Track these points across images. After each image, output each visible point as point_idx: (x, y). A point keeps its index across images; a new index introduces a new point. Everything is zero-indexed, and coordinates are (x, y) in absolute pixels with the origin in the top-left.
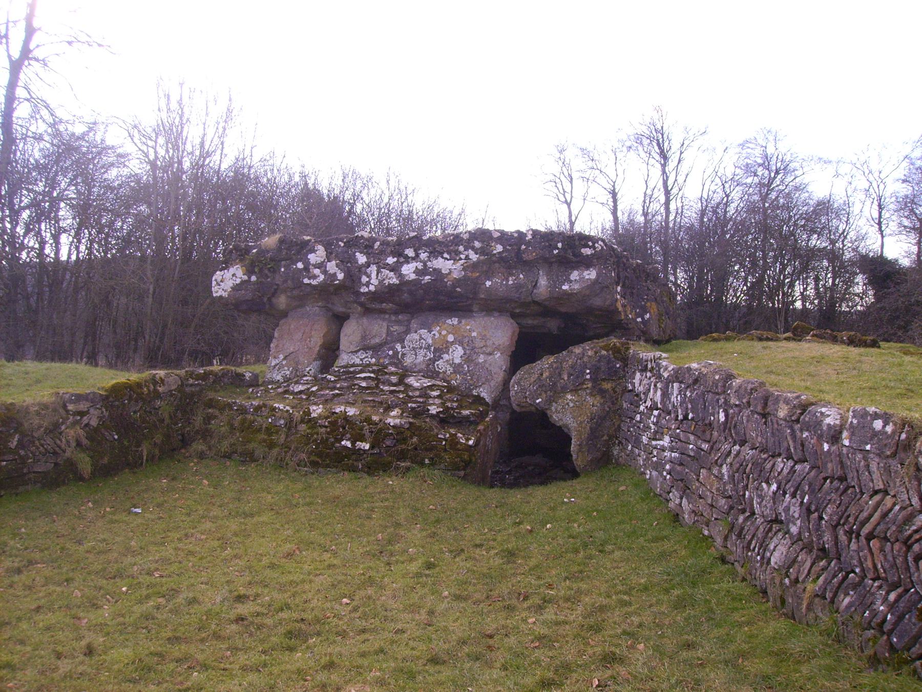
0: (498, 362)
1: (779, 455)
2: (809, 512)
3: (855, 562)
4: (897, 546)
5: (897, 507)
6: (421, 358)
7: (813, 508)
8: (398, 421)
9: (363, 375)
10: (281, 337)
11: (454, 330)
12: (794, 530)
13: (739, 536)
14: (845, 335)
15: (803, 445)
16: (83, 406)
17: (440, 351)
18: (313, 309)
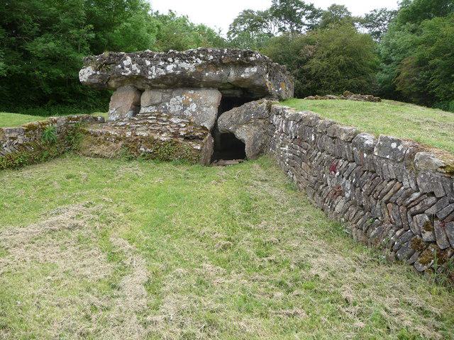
0: (213, 111)
1: (341, 158)
2: (355, 186)
3: (379, 214)
4: (401, 207)
5: (402, 188)
6: (177, 109)
7: (358, 185)
8: (165, 139)
9: (150, 117)
10: (114, 100)
11: (192, 96)
12: (347, 195)
13: (320, 195)
14: (367, 97)
15: (353, 154)
16: (13, 135)
17: (186, 105)
18: (128, 87)
